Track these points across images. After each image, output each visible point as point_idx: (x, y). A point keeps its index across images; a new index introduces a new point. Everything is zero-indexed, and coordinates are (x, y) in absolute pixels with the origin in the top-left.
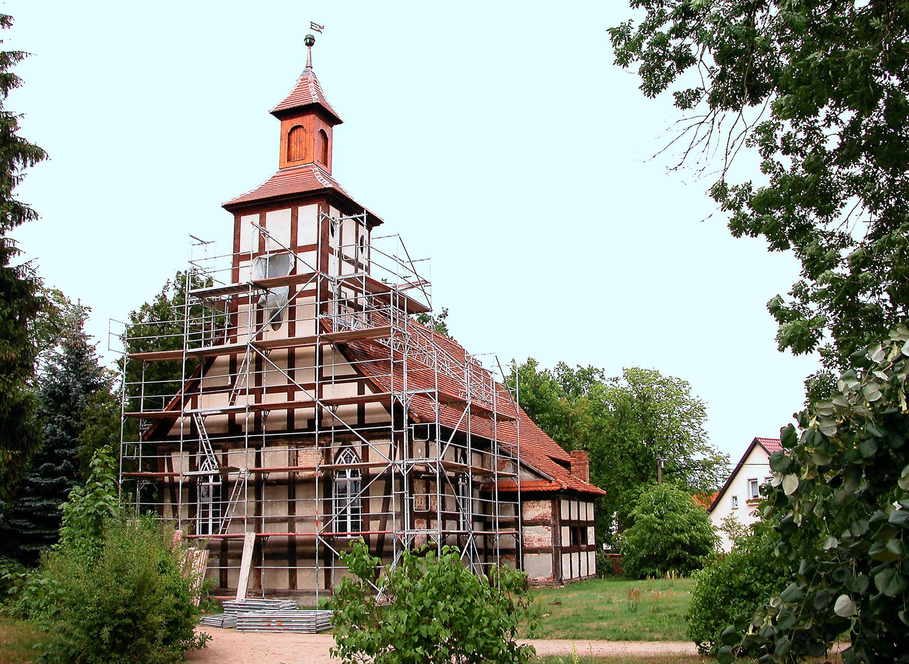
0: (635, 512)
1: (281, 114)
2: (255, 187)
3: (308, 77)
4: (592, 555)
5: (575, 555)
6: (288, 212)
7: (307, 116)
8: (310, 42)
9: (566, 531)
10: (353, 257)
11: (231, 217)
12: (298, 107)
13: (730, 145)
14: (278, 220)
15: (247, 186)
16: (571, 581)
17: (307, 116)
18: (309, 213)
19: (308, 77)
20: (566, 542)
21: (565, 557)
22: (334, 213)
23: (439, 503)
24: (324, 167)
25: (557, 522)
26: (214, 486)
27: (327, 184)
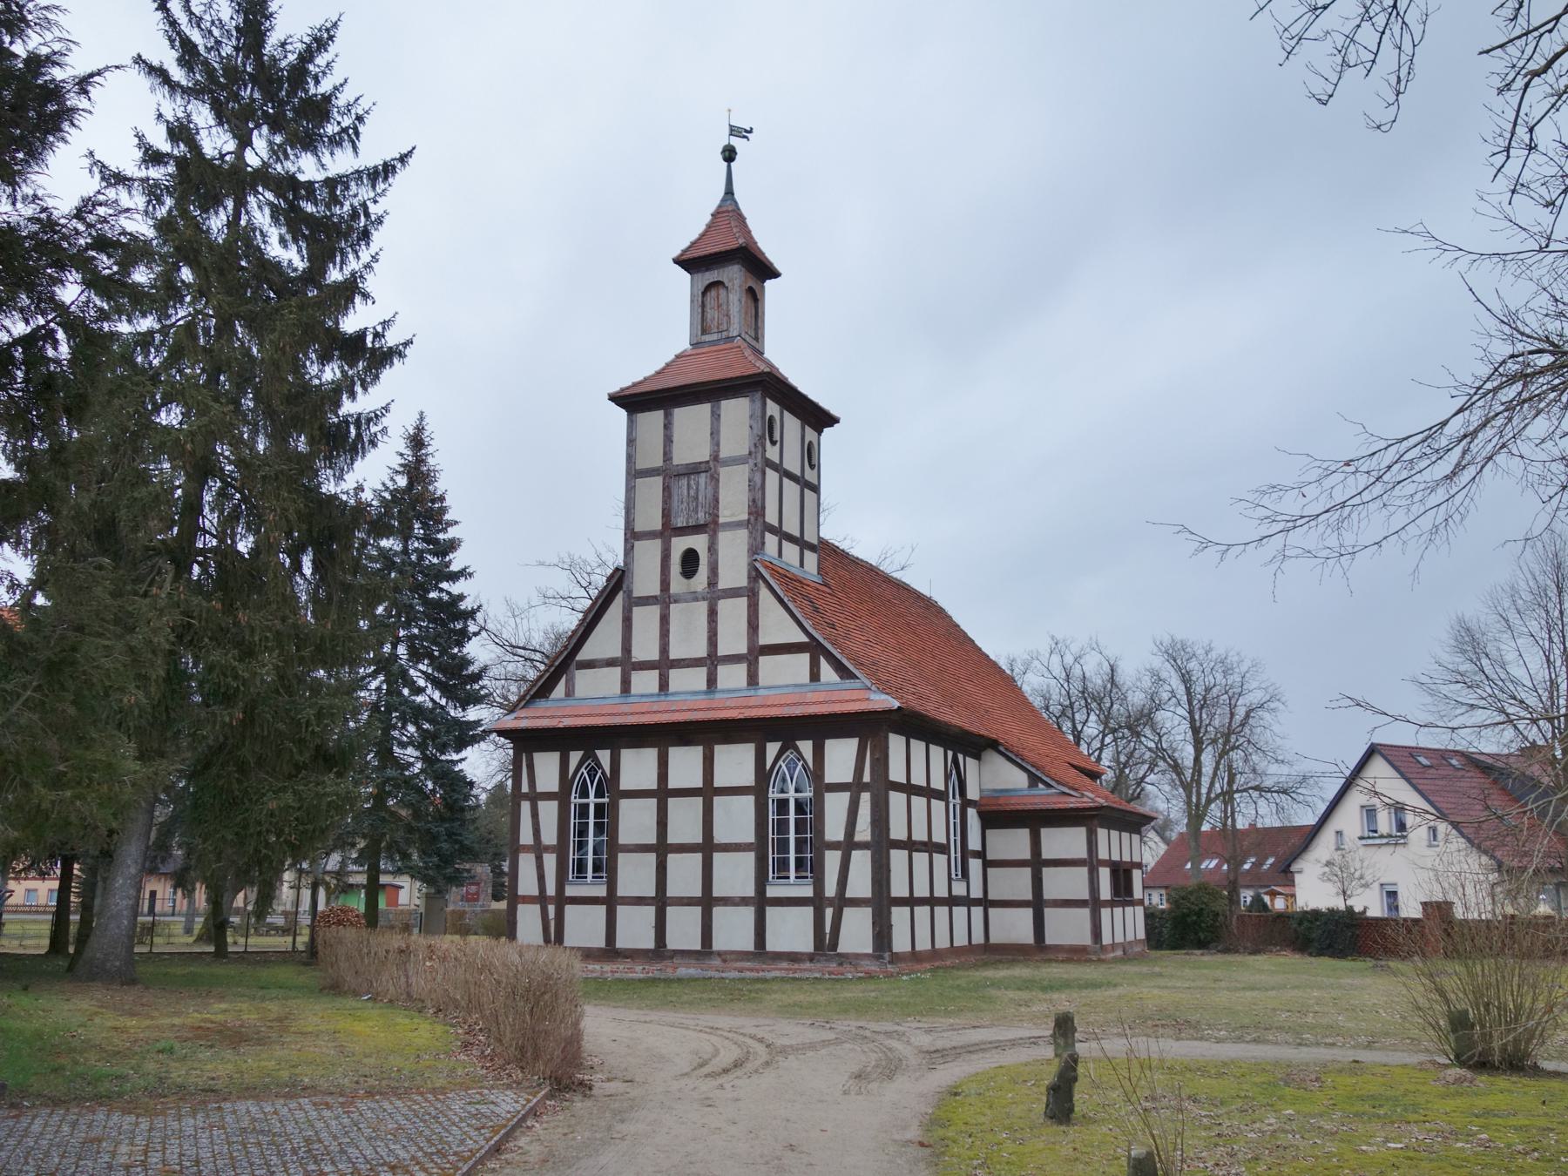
0: (1496, 1044)
1: (689, 262)
2: (650, 371)
3: (728, 212)
4: (1140, 910)
5: (1118, 911)
6: (705, 408)
7: (729, 262)
8: (729, 154)
9: (1105, 874)
10: (798, 472)
11: (622, 414)
12: (716, 254)
13: (1357, 500)
14: (691, 420)
15: (639, 368)
16: (915, 956)
17: (729, 262)
18: (737, 410)
19: (728, 212)
20: (1105, 893)
21: (1105, 913)
22: (773, 408)
23: (1529, 1000)
24: (754, 343)
25: (1091, 863)
26: (597, 805)
27: (763, 368)
